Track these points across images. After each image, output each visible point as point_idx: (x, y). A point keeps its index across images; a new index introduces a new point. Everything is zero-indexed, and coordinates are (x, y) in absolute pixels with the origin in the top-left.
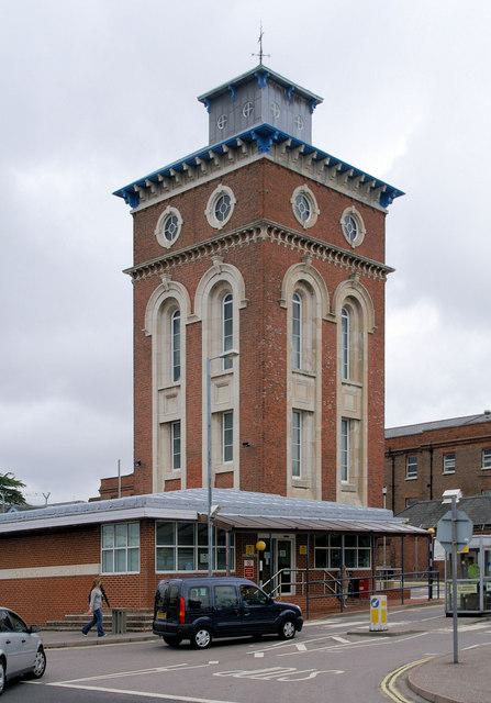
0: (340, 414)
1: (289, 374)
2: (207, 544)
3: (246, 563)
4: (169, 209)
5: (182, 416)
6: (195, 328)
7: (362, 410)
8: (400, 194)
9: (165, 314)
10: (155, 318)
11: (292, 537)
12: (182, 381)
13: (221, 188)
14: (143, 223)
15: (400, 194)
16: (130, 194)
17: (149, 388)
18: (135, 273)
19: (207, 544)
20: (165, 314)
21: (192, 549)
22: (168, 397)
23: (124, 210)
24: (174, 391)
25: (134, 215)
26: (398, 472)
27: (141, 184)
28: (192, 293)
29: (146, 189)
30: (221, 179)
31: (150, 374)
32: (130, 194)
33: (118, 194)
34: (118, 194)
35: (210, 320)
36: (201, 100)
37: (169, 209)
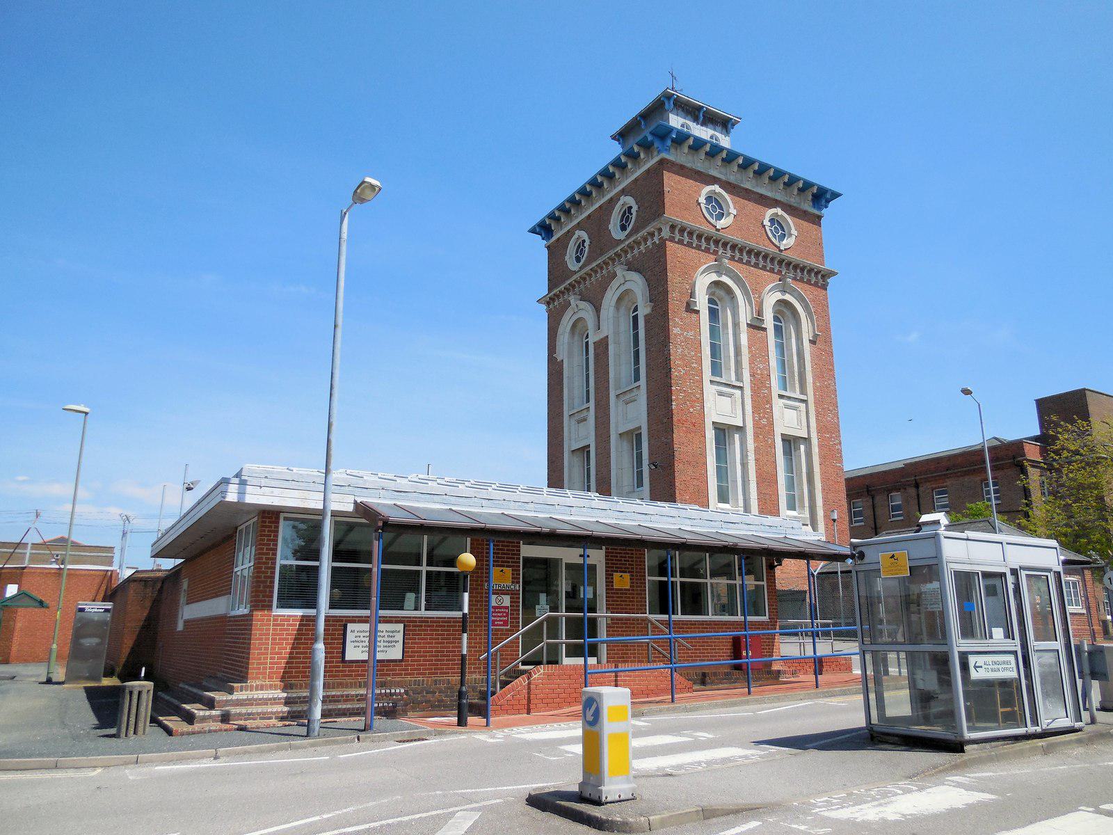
0: (779, 430)
1: (706, 384)
2: (711, 577)
3: (494, 600)
4: (578, 233)
5: (591, 441)
6: (602, 345)
7: (808, 427)
8: (836, 195)
9: (576, 338)
10: (566, 340)
11: (597, 557)
12: (592, 404)
13: (623, 199)
14: (555, 254)
15: (836, 195)
16: (544, 229)
17: (561, 414)
18: (549, 301)
19: (384, 572)
20: (576, 338)
21: (712, 584)
22: (579, 422)
23: (539, 246)
24: (585, 414)
25: (548, 247)
26: (879, 512)
27: (552, 216)
28: (598, 309)
29: (558, 219)
30: (624, 192)
31: (562, 400)
32: (544, 229)
33: (533, 231)
34: (533, 231)
35: (616, 333)
36: (614, 138)
37: (578, 233)
